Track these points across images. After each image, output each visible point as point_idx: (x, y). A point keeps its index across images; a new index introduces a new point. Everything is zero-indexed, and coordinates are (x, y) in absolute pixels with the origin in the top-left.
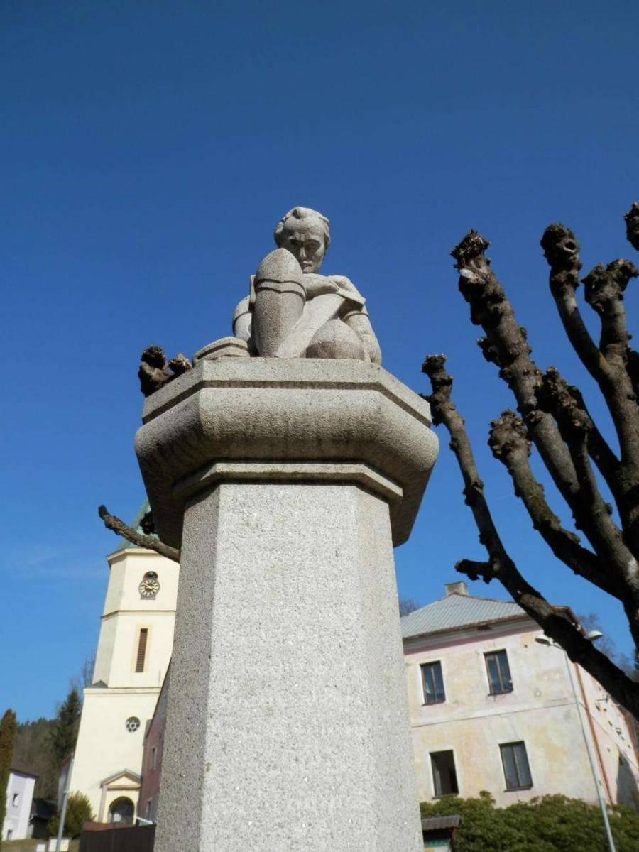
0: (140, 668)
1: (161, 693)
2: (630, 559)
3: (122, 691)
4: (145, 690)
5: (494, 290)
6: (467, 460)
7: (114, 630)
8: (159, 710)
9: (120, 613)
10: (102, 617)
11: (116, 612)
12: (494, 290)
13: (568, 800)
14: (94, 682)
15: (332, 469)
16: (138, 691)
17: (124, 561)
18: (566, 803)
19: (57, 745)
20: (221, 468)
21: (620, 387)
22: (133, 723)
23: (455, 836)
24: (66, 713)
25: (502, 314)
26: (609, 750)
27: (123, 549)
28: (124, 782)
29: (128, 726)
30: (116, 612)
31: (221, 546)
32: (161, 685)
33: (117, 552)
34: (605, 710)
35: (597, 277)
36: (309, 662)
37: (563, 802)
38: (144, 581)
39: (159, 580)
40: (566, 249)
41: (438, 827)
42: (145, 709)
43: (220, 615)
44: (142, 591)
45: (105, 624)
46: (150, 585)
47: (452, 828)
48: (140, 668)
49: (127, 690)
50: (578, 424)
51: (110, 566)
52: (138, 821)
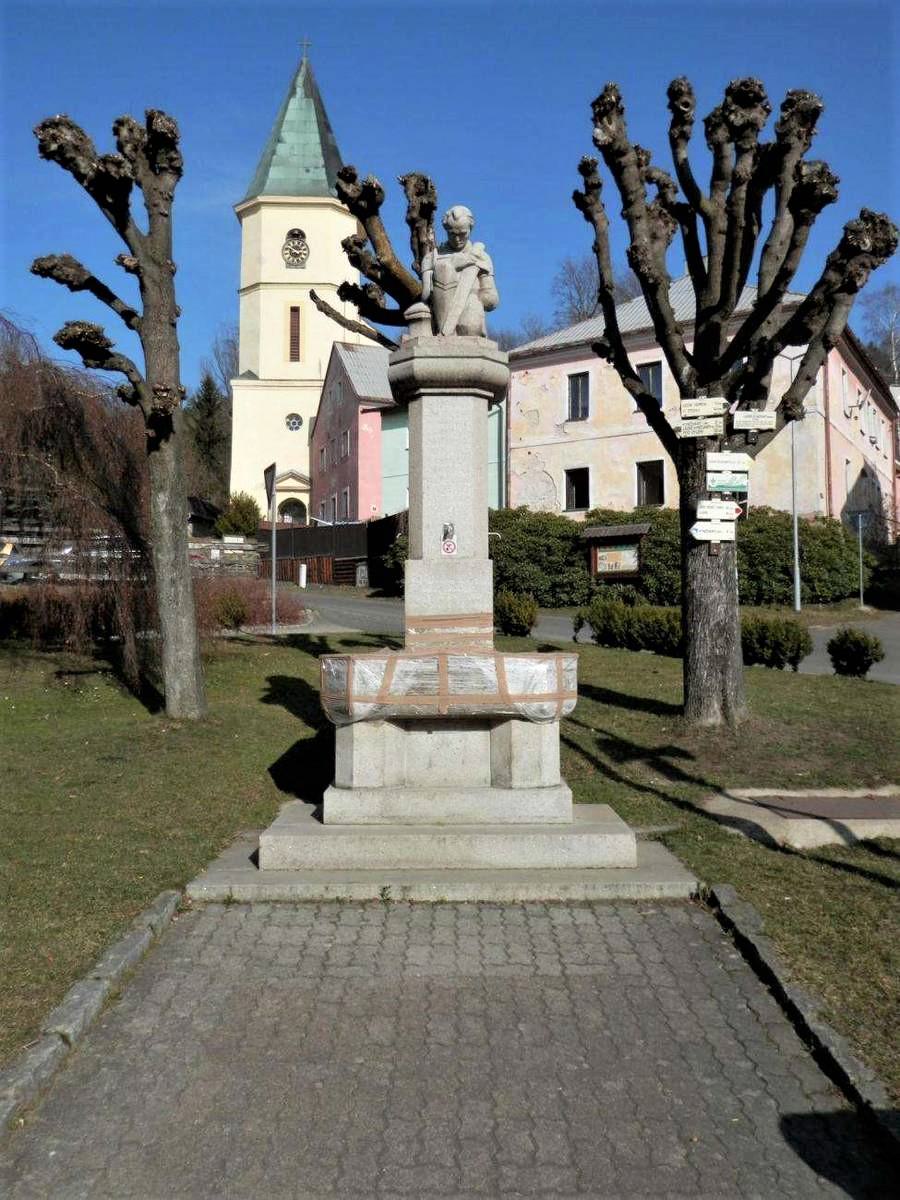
0: (295, 356)
1: (324, 386)
2: (685, 365)
3: (277, 384)
4: (304, 383)
5: (620, 147)
6: (603, 263)
7: (257, 310)
8: (323, 407)
9: (261, 287)
10: (239, 291)
11: (256, 286)
12: (620, 147)
13: (774, 511)
14: (240, 373)
15: (465, 390)
16: (296, 384)
17: (258, 213)
18: (771, 514)
19: (199, 440)
20: (422, 390)
21: (717, 223)
22: (294, 421)
23: (643, 542)
24: (203, 403)
25: (625, 167)
26: (848, 462)
27: (254, 197)
28: (291, 483)
29: (288, 423)
30: (256, 286)
31: (424, 421)
32: (324, 377)
33: (243, 202)
34: (856, 418)
35: (713, 119)
36: (454, 463)
37: (767, 513)
38: (287, 243)
39: (308, 240)
40: (682, 108)
41: (627, 534)
42: (308, 404)
43: (425, 447)
44: (288, 256)
45: (245, 301)
46: (297, 248)
47: (642, 535)
48: (295, 356)
49: (282, 383)
50: (651, 281)
51: (241, 222)
52: (311, 521)
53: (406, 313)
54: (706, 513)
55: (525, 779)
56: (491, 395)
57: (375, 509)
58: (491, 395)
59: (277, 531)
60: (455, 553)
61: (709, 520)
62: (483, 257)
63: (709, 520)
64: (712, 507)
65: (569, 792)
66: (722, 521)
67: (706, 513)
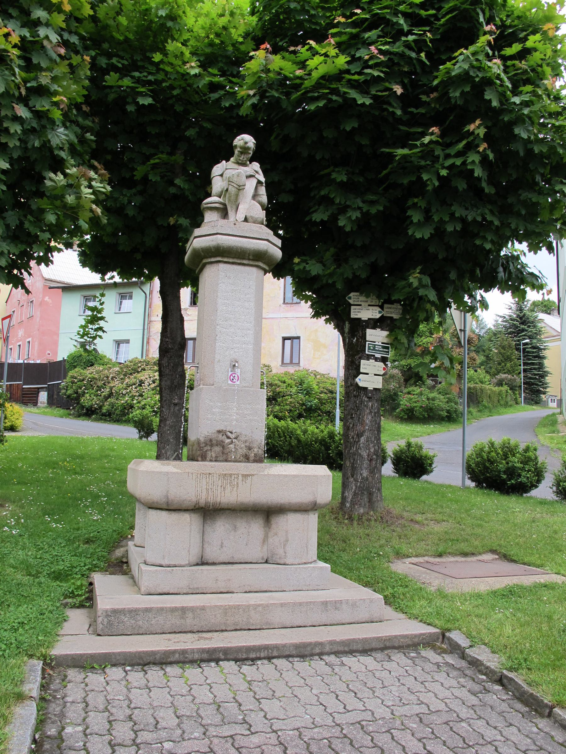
57: (49, 354)
61: (367, 374)
63: (367, 374)
66: (375, 375)
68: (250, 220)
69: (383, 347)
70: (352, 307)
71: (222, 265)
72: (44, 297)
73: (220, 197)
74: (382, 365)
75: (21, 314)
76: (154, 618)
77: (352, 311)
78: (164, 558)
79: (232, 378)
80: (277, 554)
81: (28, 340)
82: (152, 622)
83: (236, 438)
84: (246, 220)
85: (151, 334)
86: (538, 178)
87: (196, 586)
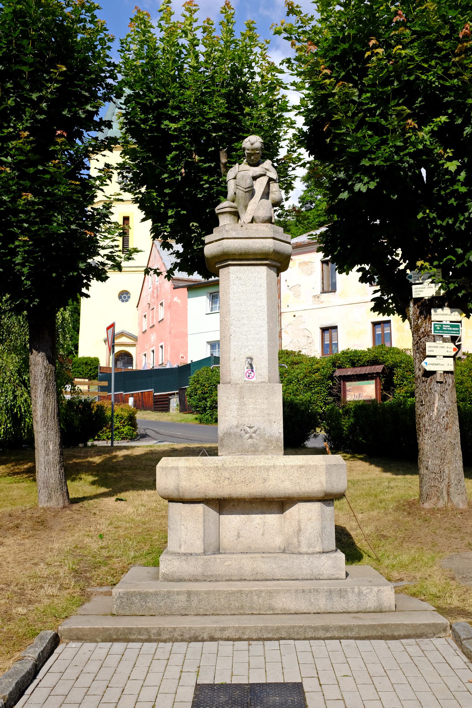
53: (217, 208)
54: (433, 351)
55: (310, 546)
56: (279, 265)
57: (182, 357)
58: (279, 265)
59: (115, 374)
60: (254, 379)
61: (435, 356)
62: (271, 170)
63: (435, 356)
64: (437, 347)
65: (343, 556)
66: (444, 357)
67: (433, 351)
68: (257, 220)
69: (452, 326)
70: (414, 287)
71: (231, 268)
72: (173, 297)
73: (233, 202)
74: (452, 345)
75: (153, 317)
76: (163, 600)
77: (413, 290)
78: (180, 547)
79: (248, 374)
80: (292, 544)
81: (160, 345)
82: (161, 604)
83: (254, 432)
84: (253, 221)
85: (283, 327)
86: (328, 192)
87: (210, 573)
